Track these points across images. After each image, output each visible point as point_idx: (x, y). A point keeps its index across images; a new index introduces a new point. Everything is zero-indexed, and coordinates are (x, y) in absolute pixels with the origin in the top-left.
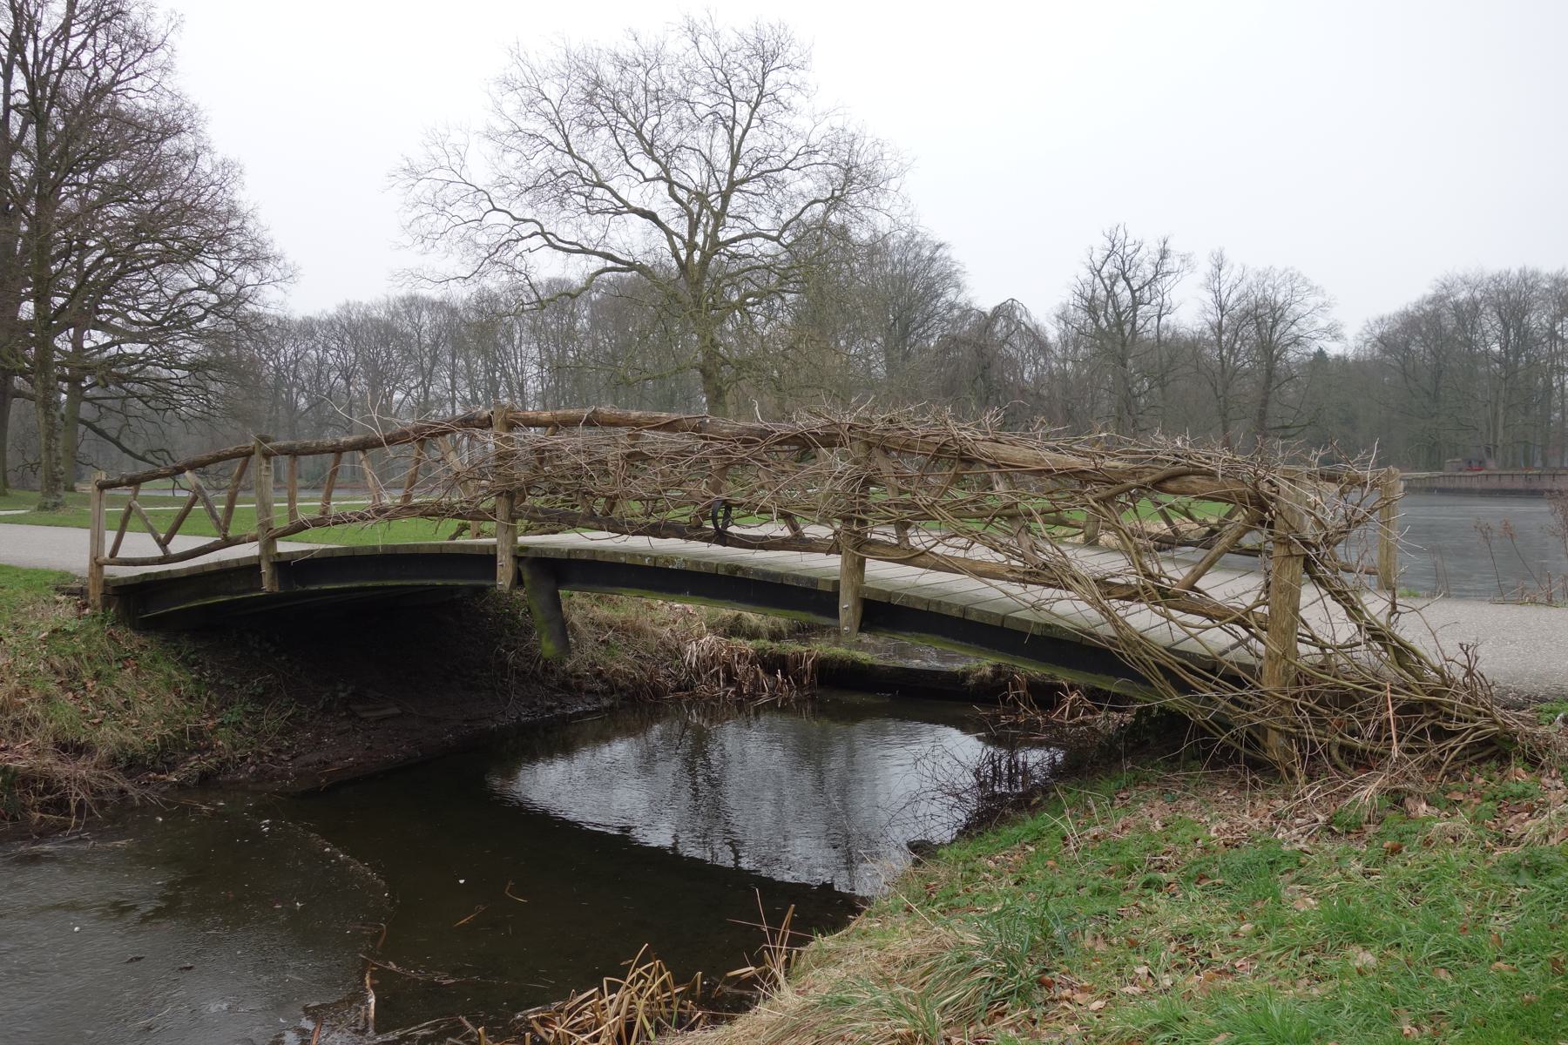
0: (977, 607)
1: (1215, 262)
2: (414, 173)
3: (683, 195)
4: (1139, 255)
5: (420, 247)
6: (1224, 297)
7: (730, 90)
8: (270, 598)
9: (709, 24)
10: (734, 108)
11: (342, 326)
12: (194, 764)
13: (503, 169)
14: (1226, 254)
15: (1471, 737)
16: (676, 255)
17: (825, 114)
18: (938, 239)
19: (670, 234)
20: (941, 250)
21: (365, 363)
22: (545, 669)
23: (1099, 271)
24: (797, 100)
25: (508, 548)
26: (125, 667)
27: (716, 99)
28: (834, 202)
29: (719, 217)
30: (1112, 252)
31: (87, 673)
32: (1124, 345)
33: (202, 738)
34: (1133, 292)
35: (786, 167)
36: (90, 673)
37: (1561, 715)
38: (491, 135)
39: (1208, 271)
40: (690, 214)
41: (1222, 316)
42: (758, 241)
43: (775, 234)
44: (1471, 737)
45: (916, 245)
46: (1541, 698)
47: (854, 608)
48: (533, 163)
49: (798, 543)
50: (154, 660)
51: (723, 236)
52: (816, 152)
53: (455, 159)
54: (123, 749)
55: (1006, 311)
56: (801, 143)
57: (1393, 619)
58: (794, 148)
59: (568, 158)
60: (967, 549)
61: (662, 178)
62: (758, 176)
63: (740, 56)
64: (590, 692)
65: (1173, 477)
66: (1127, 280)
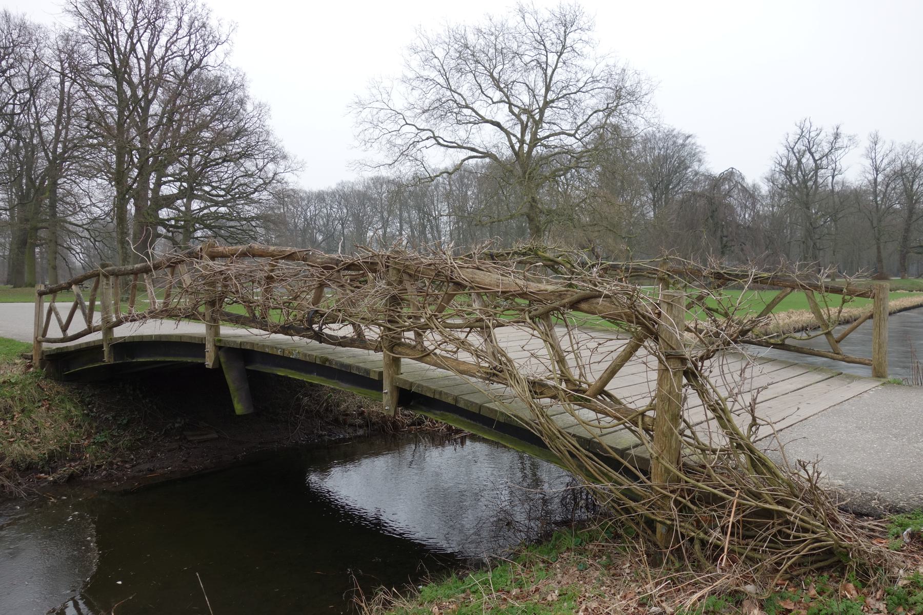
0: (466, 397)
1: (872, 140)
2: (361, 104)
3: (516, 110)
4: (820, 137)
5: (364, 147)
6: (878, 162)
7: (544, 45)
8: (109, 367)
9: (531, 6)
10: (547, 56)
11: (340, 195)
12: (64, 471)
13: (412, 100)
14: (880, 134)
15: (807, 549)
16: (512, 146)
17: (603, 57)
18: (687, 132)
19: (508, 134)
20: (690, 139)
21: (353, 215)
22: (327, 409)
23: (793, 149)
24: (586, 50)
25: (211, 340)
26: (43, 406)
27: (536, 52)
28: (609, 111)
29: (538, 124)
30: (801, 136)
31: (17, 410)
32: (808, 195)
33: (79, 452)
34: (815, 161)
35: (579, 91)
36: (19, 409)
37: (909, 530)
38: (405, 80)
39: (868, 146)
40: (522, 122)
41: (877, 175)
42: (562, 136)
43: (573, 132)
44: (807, 549)
45: (674, 136)
46: (900, 508)
47: (392, 393)
48: (428, 96)
49: (359, 341)
50: (62, 401)
51: (541, 134)
52: (598, 81)
53: (385, 96)
54: (24, 458)
55: (730, 176)
56: (589, 75)
57: (754, 429)
58: (585, 79)
59: (448, 93)
60: (455, 352)
61: (504, 101)
62: (563, 97)
63: (551, 25)
64: (351, 425)
65: (585, 299)
66: (812, 154)
